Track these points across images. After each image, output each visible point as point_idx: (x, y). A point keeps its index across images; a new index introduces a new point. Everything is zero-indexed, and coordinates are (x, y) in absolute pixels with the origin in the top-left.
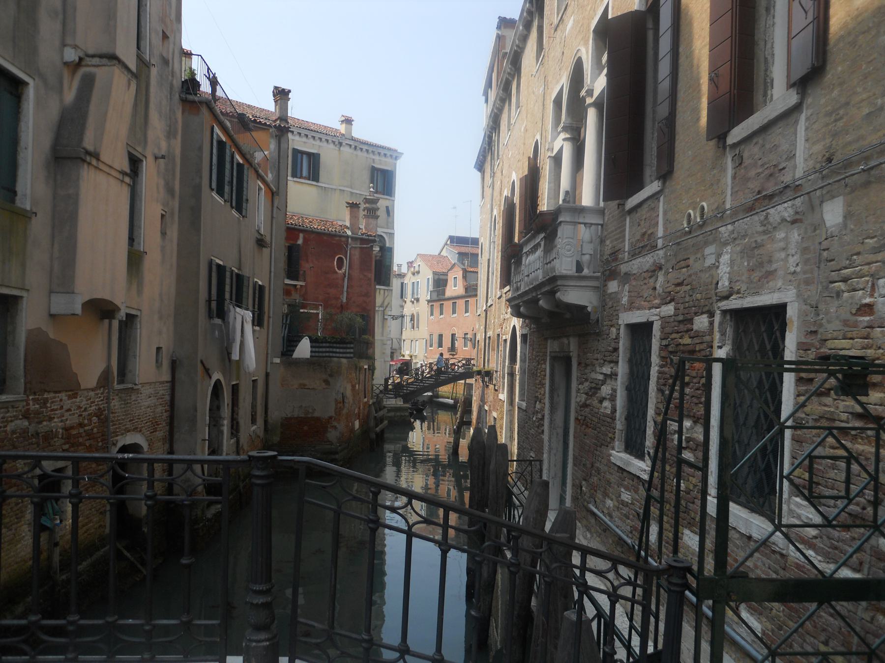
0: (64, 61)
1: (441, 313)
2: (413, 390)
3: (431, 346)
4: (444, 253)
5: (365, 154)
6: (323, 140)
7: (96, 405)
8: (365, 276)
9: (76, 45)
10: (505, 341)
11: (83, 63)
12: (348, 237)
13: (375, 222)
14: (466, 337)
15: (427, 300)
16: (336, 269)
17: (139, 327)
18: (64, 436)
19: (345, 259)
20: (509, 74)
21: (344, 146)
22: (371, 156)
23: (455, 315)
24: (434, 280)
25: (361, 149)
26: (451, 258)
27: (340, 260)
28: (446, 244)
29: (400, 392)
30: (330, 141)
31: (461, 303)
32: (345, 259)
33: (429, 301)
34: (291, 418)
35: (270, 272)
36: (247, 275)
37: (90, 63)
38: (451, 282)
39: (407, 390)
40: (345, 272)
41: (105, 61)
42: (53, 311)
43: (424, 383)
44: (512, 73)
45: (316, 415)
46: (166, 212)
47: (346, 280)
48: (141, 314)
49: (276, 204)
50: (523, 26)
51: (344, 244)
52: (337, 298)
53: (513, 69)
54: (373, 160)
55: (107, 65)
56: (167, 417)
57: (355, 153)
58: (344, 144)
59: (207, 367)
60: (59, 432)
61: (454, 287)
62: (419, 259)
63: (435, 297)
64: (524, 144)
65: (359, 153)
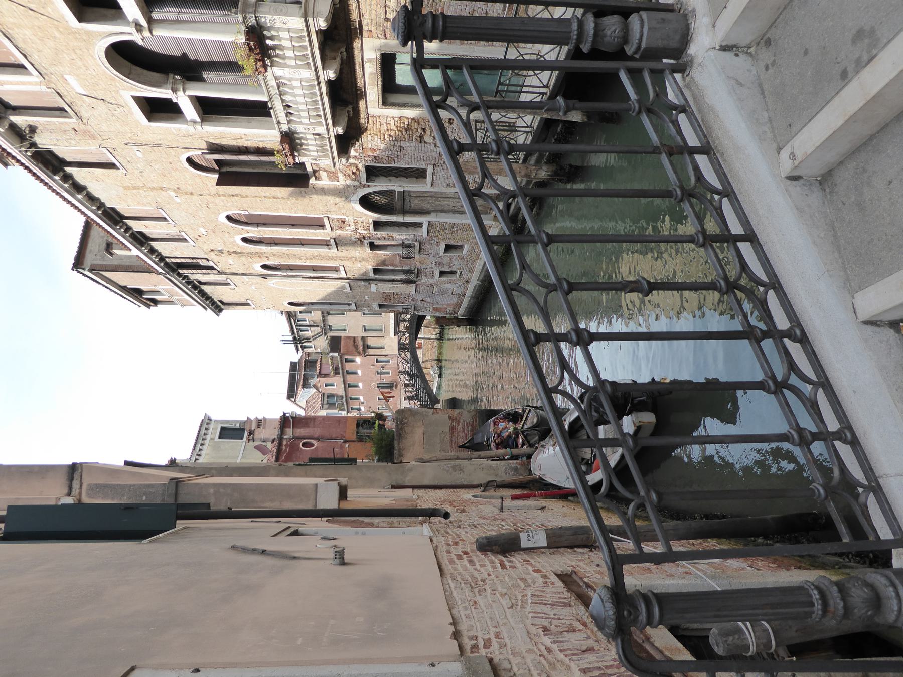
5: (205, 447)
22: (207, 442)
25: (200, 450)
28: (295, 402)
37: (78, 491)
38: (330, 390)
39: (427, 401)
44: (125, 227)
50: (78, 194)
53: (121, 224)
54: (211, 439)
55: (81, 473)
64: (192, 194)
65: (202, 453)
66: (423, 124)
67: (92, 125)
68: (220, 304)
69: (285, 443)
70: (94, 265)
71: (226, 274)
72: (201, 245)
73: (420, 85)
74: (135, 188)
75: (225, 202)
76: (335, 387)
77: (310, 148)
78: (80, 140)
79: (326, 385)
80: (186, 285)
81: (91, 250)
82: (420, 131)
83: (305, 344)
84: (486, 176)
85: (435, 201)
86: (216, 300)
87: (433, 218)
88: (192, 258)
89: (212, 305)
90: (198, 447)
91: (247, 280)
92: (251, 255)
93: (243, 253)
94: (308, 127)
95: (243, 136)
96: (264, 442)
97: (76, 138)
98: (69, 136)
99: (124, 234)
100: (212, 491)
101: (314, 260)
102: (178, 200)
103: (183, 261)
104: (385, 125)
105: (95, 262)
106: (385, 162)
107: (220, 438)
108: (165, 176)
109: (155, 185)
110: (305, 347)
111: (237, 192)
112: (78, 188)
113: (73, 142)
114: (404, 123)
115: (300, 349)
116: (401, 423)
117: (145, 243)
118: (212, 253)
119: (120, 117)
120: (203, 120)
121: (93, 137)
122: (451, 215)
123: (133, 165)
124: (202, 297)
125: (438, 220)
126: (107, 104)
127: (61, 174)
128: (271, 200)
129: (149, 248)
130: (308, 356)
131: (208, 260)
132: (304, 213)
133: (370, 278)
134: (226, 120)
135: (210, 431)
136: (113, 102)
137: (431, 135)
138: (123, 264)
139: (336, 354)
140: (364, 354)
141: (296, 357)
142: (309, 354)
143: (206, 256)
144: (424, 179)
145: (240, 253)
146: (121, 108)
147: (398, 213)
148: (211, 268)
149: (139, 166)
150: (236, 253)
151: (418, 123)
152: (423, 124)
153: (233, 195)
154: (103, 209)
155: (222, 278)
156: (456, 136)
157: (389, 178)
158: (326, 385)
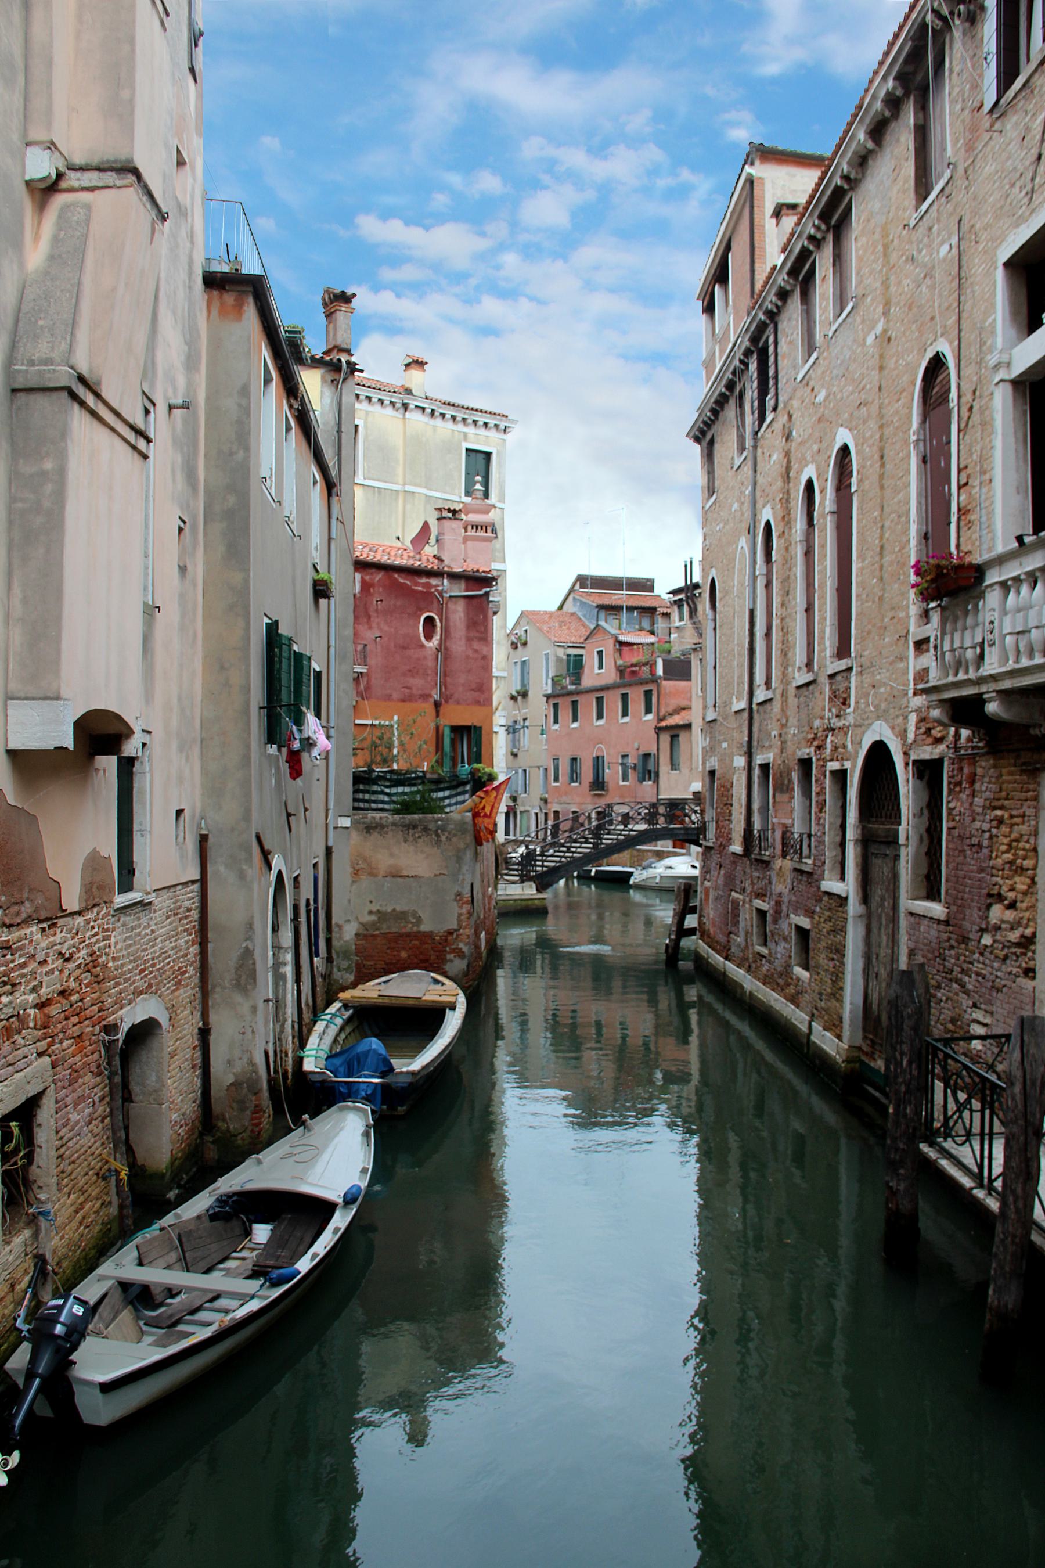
0: (27, 178)
2: (554, 867)
3: (556, 779)
5: (450, 425)
6: (375, 400)
7: (87, 946)
8: (476, 651)
9: (53, 143)
10: (840, 777)
11: (63, 185)
15: (545, 696)
16: (423, 639)
17: (148, 769)
18: (39, 1023)
19: (438, 621)
20: (811, 238)
21: (412, 410)
22: (461, 427)
25: (443, 415)
26: (584, 616)
27: (429, 621)
28: (572, 590)
29: (530, 871)
30: (387, 402)
31: (613, 701)
33: (548, 697)
35: (329, 647)
36: (308, 654)
38: (591, 663)
39: (543, 866)
41: (110, 178)
42: (12, 746)
43: (573, 852)
44: (819, 236)
45: (424, 928)
46: (184, 522)
48: (151, 740)
49: (334, 516)
50: (866, 133)
53: (823, 227)
54: (465, 435)
56: (195, 954)
57: (432, 422)
58: (412, 407)
59: (266, 847)
60: (29, 1015)
64: (881, 368)
65: (438, 422)
66: (1024, 905)
67: (992, 143)
68: (708, 437)
69: (434, 581)
70: (763, 184)
71: (755, 447)
72: (799, 394)
74: (886, 247)
75: (871, 442)
77: (957, 636)
78: (963, 121)
79: (600, 653)
80: (731, 369)
81: (794, 176)
82: (1011, 895)
83: (686, 608)
85: (887, 915)
86: (715, 429)
87: (854, 907)
88: (776, 377)
89: (704, 423)
90: (449, 412)
91: (747, 492)
92: (786, 500)
93: (789, 483)
94: (996, 631)
95: (987, 477)
96: (437, 541)
97: (967, 112)
98: (969, 96)
99: (805, 235)
100: (48, 465)
101: (781, 634)
102: (870, 340)
103: (772, 359)
104: (1021, 811)
105: (768, 186)
106: (951, 805)
107: (467, 450)
108: (910, 309)
109: (893, 289)
111: (888, 466)
112: (878, 131)
113: (959, 107)
114: (1024, 858)
115: (677, 598)
116: (439, 828)
117: (796, 279)
118: (786, 417)
119: (1009, 200)
120: (1017, 384)
121: (970, 147)
122: (861, 945)
123: (925, 240)
124: (716, 402)
125: (850, 921)
126: (1032, 168)
127: (899, 92)
128: (877, 542)
129: (788, 288)
130: (663, 614)
131: (775, 409)
132: (857, 615)
133: (754, 756)
134: (1020, 435)
135: (482, 432)
136: (1037, 180)
137: (1003, 922)
138: (767, 240)
139: (660, 671)
140: (659, 730)
141: (663, 590)
142: (667, 615)
143: (781, 406)
144: (924, 893)
145: (788, 477)
146: (1026, 200)
147: (864, 828)
148: (762, 418)
149: (924, 252)
150: (788, 468)
151: (1025, 893)
152: (1024, 905)
153: (882, 457)
154: (846, 187)
155: (749, 443)
156: (1003, 982)
157: (926, 812)
158: (600, 653)
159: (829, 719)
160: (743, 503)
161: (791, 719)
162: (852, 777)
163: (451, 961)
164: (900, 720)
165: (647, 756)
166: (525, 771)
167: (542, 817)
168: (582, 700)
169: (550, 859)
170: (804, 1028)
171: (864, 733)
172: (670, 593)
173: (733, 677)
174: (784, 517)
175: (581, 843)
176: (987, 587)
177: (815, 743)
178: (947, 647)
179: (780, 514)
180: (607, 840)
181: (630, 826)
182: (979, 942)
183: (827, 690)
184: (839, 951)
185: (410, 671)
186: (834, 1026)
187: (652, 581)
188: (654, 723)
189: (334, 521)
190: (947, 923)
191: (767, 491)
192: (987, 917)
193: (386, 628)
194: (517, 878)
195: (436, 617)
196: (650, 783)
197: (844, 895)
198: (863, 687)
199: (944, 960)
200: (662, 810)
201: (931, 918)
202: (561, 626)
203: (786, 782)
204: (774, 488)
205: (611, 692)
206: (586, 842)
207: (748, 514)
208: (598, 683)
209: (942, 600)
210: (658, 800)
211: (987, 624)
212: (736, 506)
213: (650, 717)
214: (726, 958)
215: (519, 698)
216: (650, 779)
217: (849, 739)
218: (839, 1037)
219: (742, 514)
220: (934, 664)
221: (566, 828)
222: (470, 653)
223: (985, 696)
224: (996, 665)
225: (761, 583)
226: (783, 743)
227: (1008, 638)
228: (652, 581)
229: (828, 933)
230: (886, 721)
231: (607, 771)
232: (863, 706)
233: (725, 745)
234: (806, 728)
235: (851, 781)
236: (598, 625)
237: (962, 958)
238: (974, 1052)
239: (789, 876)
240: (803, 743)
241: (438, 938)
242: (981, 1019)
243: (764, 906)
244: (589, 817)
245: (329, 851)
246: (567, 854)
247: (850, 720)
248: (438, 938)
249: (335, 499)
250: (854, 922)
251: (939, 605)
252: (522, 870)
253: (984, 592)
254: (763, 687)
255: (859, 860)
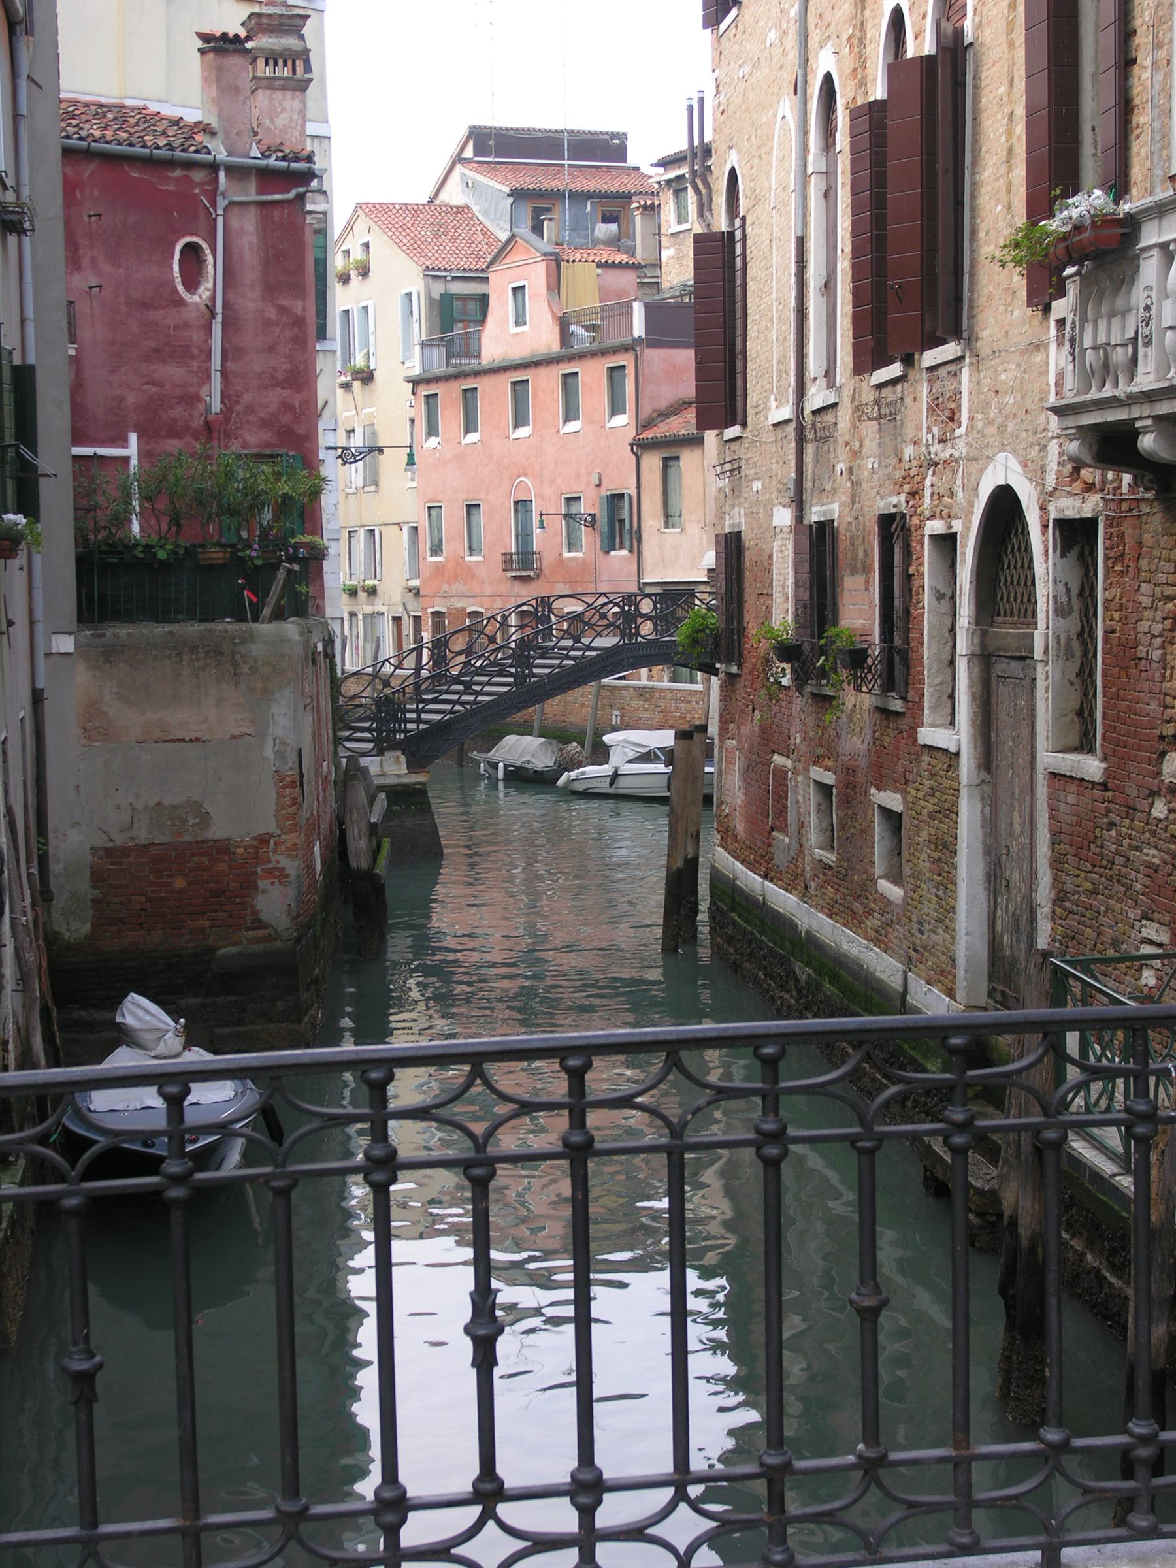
1: (470, 426)
3: (436, 550)
4: (454, 195)
8: (283, 310)
10: (947, 543)
12: (214, 167)
13: (297, 104)
14: (574, 510)
16: (180, 288)
19: (208, 251)
23: (524, 432)
24: (431, 301)
27: (192, 251)
28: (458, 159)
29: (394, 731)
32: (208, 251)
34: (125, 852)
35: (23, 321)
38: (501, 308)
39: (419, 721)
40: (213, 298)
43: (477, 693)
45: (217, 831)
47: (217, 328)
49: (24, 72)
51: (204, 192)
52: (192, 399)
61: (517, 324)
62: (361, 225)
63: (438, 361)
73: (384, 1055)
76: (514, 330)
77: (1102, 325)
79: (518, 291)
84: (719, 1093)
92: (859, 41)
94: (1154, 321)
110: (679, 192)
115: (671, 175)
125: (964, 792)
128: (1003, 139)
133: (806, 510)
139: (639, 329)
140: (641, 447)
142: (651, 210)
147: (984, 634)
158: (518, 291)
159: (928, 446)
160: (785, 33)
161: (867, 442)
162: (964, 546)
163: (264, 891)
164: (1034, 453)
165: (615, 499)
166: (372, 532)
167: (408, 627)
168: (483, 385)
169: (431, 706)
170: (896, 983)
171: (982, 471)
172: (658, 165)
173: (769, 361)
174: (855, 70)
175: (491, 675)
176: (1143, 250)
177: (907, 488)
178: (1088, 342)
179: (849, 64)
180: (542, 668)
181: (586, 641)
182: (1149, 813)
183: (925, 392)
184: (946, 847)
185: (157, 351)
186: (944, 978)
187: (622, 137)
188: (631, 433)
189: (23, 84)
190: (1104, 786)
191: (827, 17)
192: (1159, 773)
193: (108, 268)
194: (370, 746)
195: (204, 245)
196: (625, 552)
197: (953, 749)
198: (980, 393)
199: (1102, 846)
200: (646, 606)
201: (1082, 780)
202: (437, 235)
203: (861, 554)
204: (838, 13)
205: (543, 372)
206: (500, 674)
207: (793, 55)
208: (519, 352)
209: (1082, 265)
210: (642, 586)
211: (1141, 310)
212: (773, 36)
213: (621, 420)
214: (765, 876)
215: (357, 385)
216: (622, 547)
217: (959, 482)
218: (950, 993)
219: (784, 53)
220: (1070, 367)
221: (457, 648)
222: (271, 313)
223: (1138, 424)
224: (1152, 377)
225: (815, 189)
226: (856, 484)
227: (1169, 333)
228: (622, 137)
229: (931, 817)
230: (1014, 452)
231: (537, 531)
232: (980, 425)
233: (757, 485)
234: (893, 461)
235: (963, 554)
236: (513, 236)
237: (1126, 841)
238: (1145, 990)
239: (865, 719)
240: (889, 487)
241: (240, 851)
242: (1154, 937)
243: (829, 778)
244: (504, 623)
245: (37, 697)
246: (464, 698)
247: (961, 449)
248: (240, 851)
249: (23, 41)
250: (970, 796)
251: (1078, 273)
252: (377, 730)
253: (1138, 256)
254: (822, 382)
255: (977, 689)
